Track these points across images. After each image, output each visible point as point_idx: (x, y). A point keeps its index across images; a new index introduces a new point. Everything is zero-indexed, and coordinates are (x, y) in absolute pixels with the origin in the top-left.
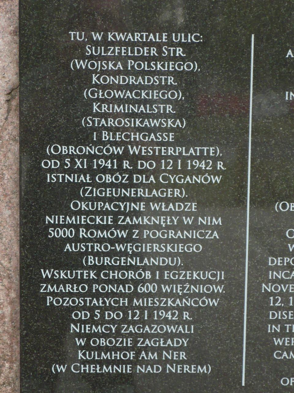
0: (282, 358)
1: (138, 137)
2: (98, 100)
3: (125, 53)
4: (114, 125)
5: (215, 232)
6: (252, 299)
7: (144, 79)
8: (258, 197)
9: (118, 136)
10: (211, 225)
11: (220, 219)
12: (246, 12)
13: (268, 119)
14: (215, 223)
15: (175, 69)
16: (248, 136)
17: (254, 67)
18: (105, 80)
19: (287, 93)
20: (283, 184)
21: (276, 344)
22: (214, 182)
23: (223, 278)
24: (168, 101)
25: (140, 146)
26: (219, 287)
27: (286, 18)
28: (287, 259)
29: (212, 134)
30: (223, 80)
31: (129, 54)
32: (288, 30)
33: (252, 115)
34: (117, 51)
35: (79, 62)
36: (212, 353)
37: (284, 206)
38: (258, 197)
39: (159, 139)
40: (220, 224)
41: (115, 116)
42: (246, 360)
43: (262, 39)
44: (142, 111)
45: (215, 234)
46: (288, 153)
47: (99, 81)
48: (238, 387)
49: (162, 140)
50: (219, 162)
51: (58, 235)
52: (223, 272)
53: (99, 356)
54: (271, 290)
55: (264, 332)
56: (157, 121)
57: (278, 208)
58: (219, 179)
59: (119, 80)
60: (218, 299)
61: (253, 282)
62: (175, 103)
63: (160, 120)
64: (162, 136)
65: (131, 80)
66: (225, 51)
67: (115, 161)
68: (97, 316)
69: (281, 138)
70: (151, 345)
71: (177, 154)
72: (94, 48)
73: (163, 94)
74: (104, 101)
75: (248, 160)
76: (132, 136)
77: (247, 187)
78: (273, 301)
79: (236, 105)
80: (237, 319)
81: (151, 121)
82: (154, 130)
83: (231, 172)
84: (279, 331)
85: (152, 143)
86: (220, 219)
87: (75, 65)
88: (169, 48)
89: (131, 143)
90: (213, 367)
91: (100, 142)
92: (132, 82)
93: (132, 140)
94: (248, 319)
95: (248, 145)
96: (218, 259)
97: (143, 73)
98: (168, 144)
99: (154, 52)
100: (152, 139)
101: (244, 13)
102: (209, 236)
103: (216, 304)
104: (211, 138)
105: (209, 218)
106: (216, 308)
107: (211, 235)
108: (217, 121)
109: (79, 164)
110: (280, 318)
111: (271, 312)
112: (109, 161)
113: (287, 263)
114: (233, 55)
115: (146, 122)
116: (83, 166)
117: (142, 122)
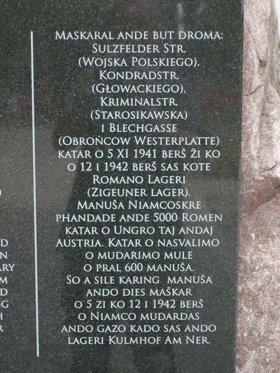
1: (143, 128)
2: (105, 94)
3: (129, 50)
4: (120, 118)
9: (124, 128)
15: (176, 65)
24: (171, 95)
25: (145, 137)
31: (133, 52)
34: (121, 49)
35: (86, 60)
39: (162, 130)
41: (121, 109)
44: (146, 104)
47: (107, 77)
51: (162, 219)
53: (128, 340)
56: (161, 113)
62: (177, 97)
64: (165, 127)
65: (136, 76)
67: (154, 150)
68: (89, 305)
70: (80, 343)
71: (180, 144)
72: (100, 46)
73: (166, 89)
76: (138, 128)
81: (155, 113)
85: (153, 135)
89: (136, 134)
91: (107, 134)
92: (137, 77)
93: (138, 131)
97: (147, 69)
109: (121, 154)
112: (149, 151)
115: (150, 115)
116: (125, 156)
117: (146, 115)
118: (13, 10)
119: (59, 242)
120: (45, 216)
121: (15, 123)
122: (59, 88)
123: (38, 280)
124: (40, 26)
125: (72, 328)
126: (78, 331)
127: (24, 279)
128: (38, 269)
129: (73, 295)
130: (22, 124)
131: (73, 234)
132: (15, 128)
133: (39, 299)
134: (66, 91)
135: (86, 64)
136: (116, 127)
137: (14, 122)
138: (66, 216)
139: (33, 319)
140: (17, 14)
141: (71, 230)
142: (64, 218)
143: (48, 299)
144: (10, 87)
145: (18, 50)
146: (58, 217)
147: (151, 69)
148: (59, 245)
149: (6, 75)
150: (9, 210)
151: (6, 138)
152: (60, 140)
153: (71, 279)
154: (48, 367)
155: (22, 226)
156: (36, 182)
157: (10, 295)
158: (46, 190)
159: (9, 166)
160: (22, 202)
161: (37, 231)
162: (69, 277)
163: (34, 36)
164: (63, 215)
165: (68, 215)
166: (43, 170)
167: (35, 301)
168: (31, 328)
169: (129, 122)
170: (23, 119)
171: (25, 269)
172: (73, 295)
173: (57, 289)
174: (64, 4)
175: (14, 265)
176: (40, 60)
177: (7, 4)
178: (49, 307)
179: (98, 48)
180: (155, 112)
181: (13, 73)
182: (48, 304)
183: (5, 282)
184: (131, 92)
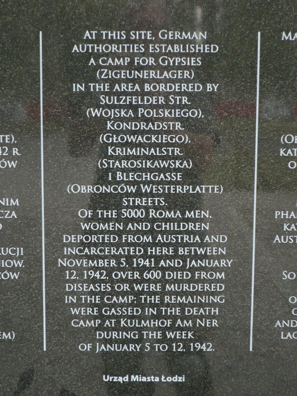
0: (79, 326)
2: (112, 144)
4: (127, 167)
5: (13, 212)
6: (50, 273)
7: (153, 125)
8: (52, 180)
10: (9, 206)
11: (17, 200)
12: (34, 11)
13: (58, 109)
14: (12, 204)
16: (40, 124)
17: (43, 62)
18: (118, 126)
19: (74, 85)
20: (74, 168)
21: (73, 313)
22: (10, 166)
23: (22, 254)
26: (19, 262)
27: (71, 16)
28: (80, 237)
29: (7, 123)
30: (15, 74)
32: (73, 27)
33: (43, 105)
34: (128, 100)
36: (15, 321)
37: (76, 188)
38: (52, 180)
40: (18, 205)
41: (127, 158)
42: (46, 327)
43: (50, 35)
45: (14, 214)
46: (77, 141)
48: (40, 351)
49: (171, 179)
50: (14, 149)
52: (22, 249)
54: (67, 264)
55: (62, 303)
57: (70, 190)
58: (15, 164)
59: (131, 126)
60: (19, 273)
61: (49, 258)
62: (182, 146)
63: (169, 161)
66: (15, 47)
69: (70, 126)
71: (185, 192)
72: (107, 97)
74: (116, 145)
75: (41, 146)
76: (144, 176)
77: (41, 171)
78: (69, 274)
79: (28, 97)
80: (36, 291)
82: (163, 170)
83: (26, 158)
84: (75, 301)
86: (17, 200)
87: (90, 112)
88: (176, 97)
89: (141, 182)
90: (16, 333)
91: (115, 182)
93: (144, 179)
94: (46, 291)
95: (40, 133)
96: (17, 236)
98: (176, 183)
99: (162, 100)
100: (162, 179)
101: (32, 12)
102: (8, 216)
103: (17, 278)
104: (6, 126)
105: (7, 199)
106: (17, 280)
107: (10, 215)
108: (11, 112)
110: (75, 290)
111: (67, 285)
113: (80, 240)
114: (24, 50)
117: (153, 164)
118: (242, 10)
119: (277, 238)
120: (264, 212)
121: (239, 121)
122: (283, 88)
123: (255, 276)
124: (268, 27)
125: (286, 323)
126: (292, 326)
127: (242, 275)
128: (255, 265)
129: (288, 290)
130: (246, 122)
131: (291, 230)
132: (239, 126)
133: (255, 294)
134: (290, 90)
135: (94, 115)
136: (123, 175)
137: (238, 120)
138: (285, 213)
139: (248, 314)
140: (246, 14)
141: (289, 227)
142: (283, 214)
143: (263, 294)
144: (236, 86)
145: (245, 50)
146: (277, 213)
147: (157, 119)
148: (277, 241)
149: (232, 74)
150: (230, 207)
151: (230, 136)
152: (282, 138)
153: (287, 274)
154: (260, 362)
155: (241, 222)
156: (258, 179)
157: (226, 290)
158: (267, 187)
159: (231, 163)
160: (242, 199)
161: (256, 227)
162: (285, 273)
163: (261, 37)
164: (282, 212)
165: (287, 212)
166: (264, 167)
167: (251, 297)
168: (246, 323)
169: (135, 170)
170: (248, 117)
171: (242, 264)
172: (288, 290)
173: (273, 285)
174: (292, 6)
175: (232, 260)
176: (266, 60)
177: (236, 4)
178: (264, 302)
179: (105, 100)
180: (160, 161)
181: (240, 73)
182: (263, 299)
183: (222, 278)
184: (137, 142)
